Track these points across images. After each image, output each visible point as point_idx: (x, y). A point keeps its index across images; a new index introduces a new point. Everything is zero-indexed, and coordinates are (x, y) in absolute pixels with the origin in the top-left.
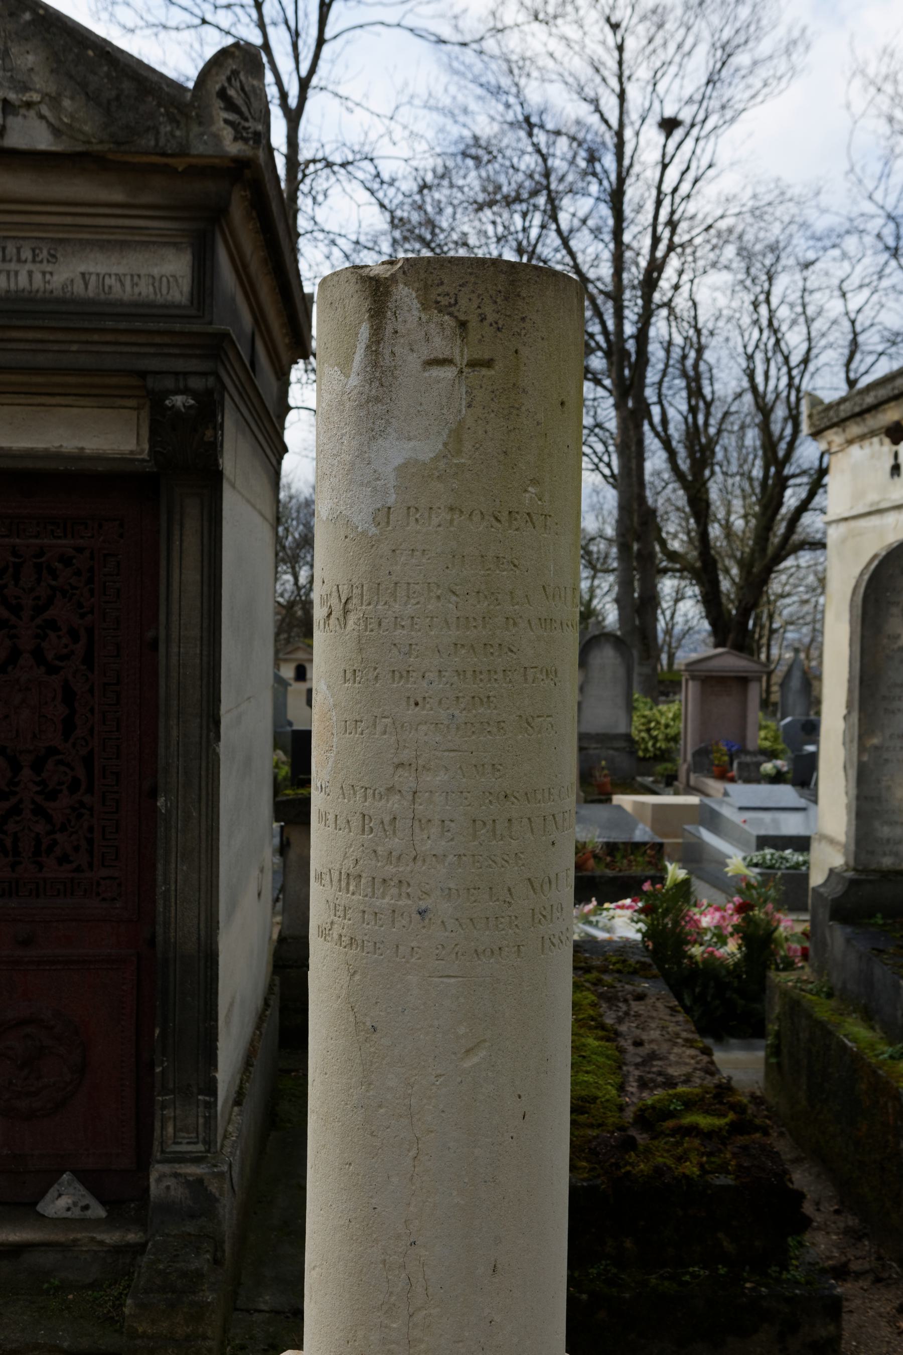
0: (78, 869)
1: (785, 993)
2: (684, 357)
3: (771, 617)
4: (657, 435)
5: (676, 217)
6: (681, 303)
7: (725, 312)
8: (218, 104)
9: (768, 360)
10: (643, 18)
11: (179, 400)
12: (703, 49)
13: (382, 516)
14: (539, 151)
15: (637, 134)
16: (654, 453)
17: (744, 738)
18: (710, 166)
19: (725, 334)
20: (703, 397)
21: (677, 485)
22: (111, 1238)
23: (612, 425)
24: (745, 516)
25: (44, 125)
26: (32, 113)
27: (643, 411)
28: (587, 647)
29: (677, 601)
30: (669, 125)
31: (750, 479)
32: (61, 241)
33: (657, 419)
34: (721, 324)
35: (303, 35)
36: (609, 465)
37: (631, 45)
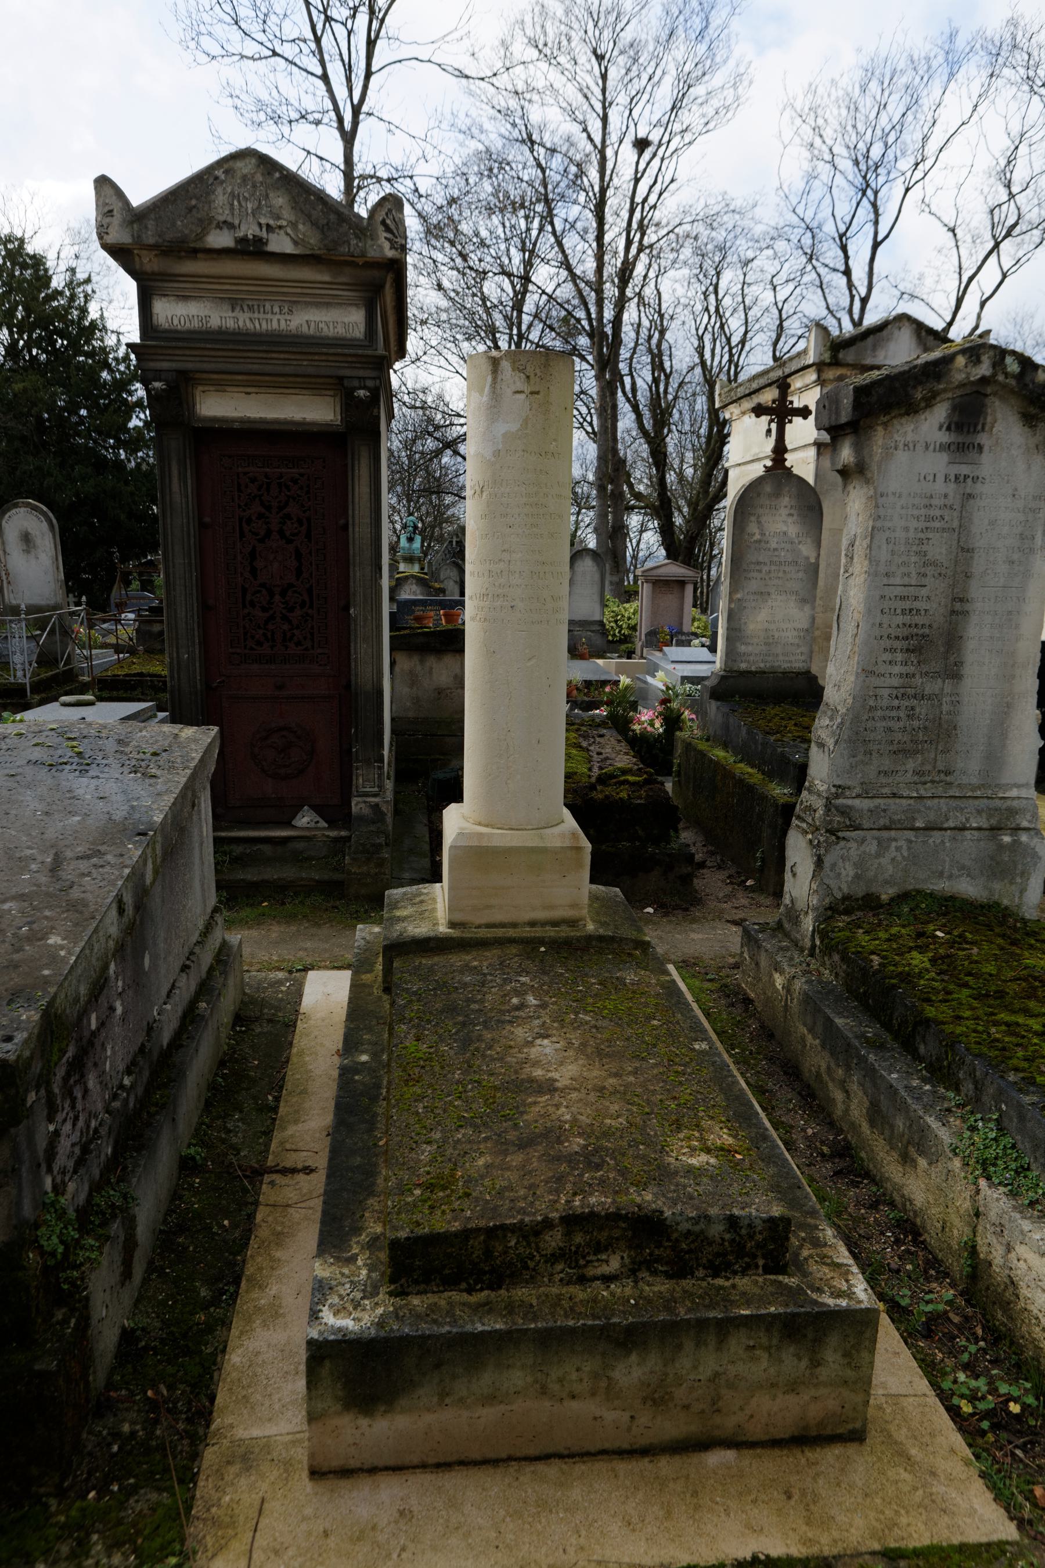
0: (306, 649)
1: (683, 741)
2: (650, 337)
3: (712, 545)
4: (628, 400)
5: (646, 222)
6: (649, 291)
7: (682, 300)
8: (381, 228)
9: (715, 340)
10: (621, 53)
11: (362, 393)
12: (668, 81)
13: (497, 453)
14: (539, 165)
15: (616, 153)
16: (625, 415)
17: (681, 624)
18: (672, 181)
19: (683, 318)
20: (663, 369)
21: (642, 441)
22: (333, 834)
23: (593, 392)
24: (695, 466)
25: (288, 239)
26: (282, 232)
27: (618, 377)
28: (576, 557)
29: (641, 532)
30: (641, 145)
31: (699, 437)
32: (295, 302)
33: (628, 387)
34: (678, 310)
35: (354, 68)
36: (591, 424)
37: (613, 74)
